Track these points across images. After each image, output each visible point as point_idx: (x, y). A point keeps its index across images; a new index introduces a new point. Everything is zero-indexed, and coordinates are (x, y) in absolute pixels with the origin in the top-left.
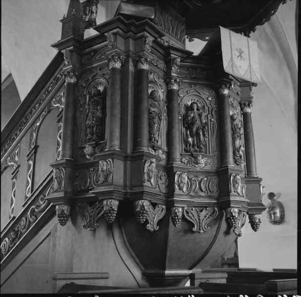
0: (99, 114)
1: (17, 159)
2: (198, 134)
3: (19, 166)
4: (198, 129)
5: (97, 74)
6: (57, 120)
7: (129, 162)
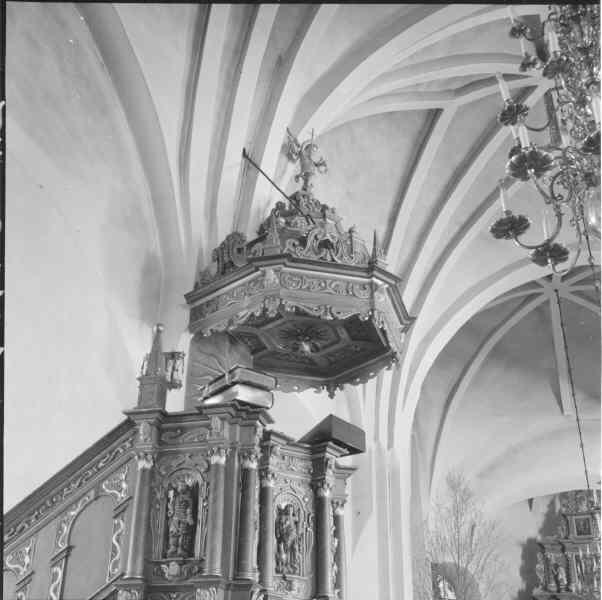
0: (189, 520)
1: (27, 560)
2: (292, 549)
3: (33, 573)
4: (293, 543)
5: (184, 462)
6: (114, 515)
7: (230, 592)
